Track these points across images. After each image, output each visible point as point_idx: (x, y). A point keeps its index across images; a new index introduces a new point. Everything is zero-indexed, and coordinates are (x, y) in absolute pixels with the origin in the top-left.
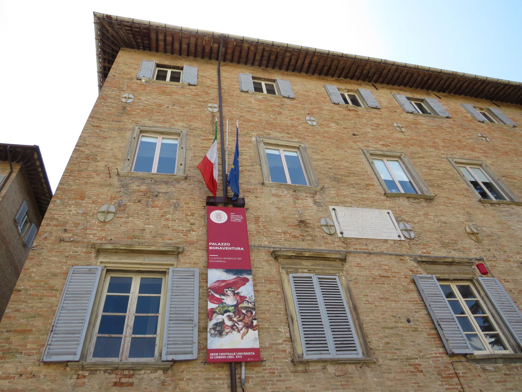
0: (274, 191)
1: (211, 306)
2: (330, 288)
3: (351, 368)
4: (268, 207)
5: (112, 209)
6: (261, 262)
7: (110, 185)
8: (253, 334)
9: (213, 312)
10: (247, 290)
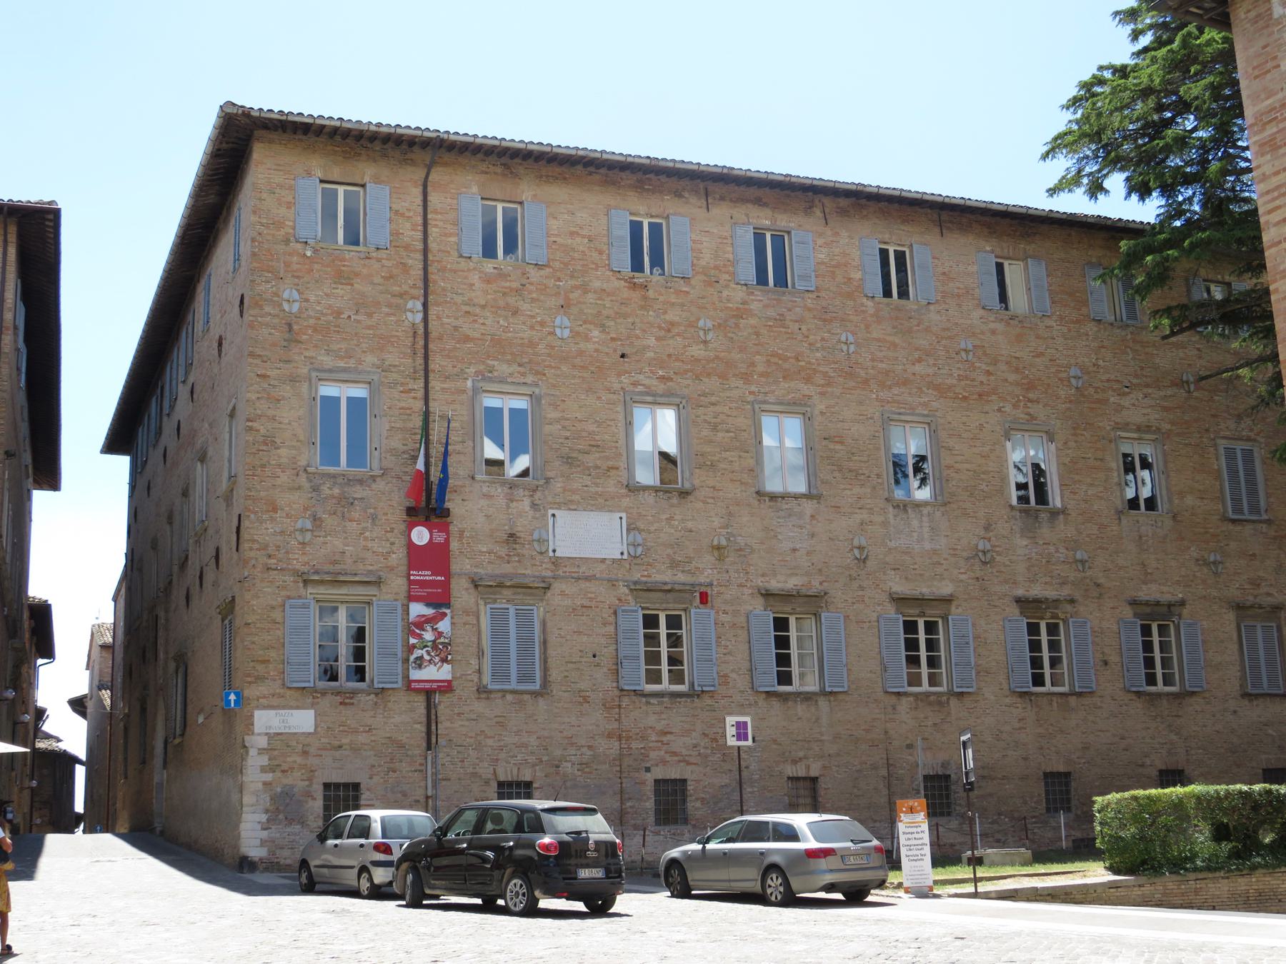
0: (485, 490)
1: (412, 641)
2: (525, 621)
3: (526, 697)
4: (471, 509)
5: (309, 526)
6: (461, 593)
7: (299, 488)
8: (447, 667)
9: (414, 646)
10: (444, 626)
